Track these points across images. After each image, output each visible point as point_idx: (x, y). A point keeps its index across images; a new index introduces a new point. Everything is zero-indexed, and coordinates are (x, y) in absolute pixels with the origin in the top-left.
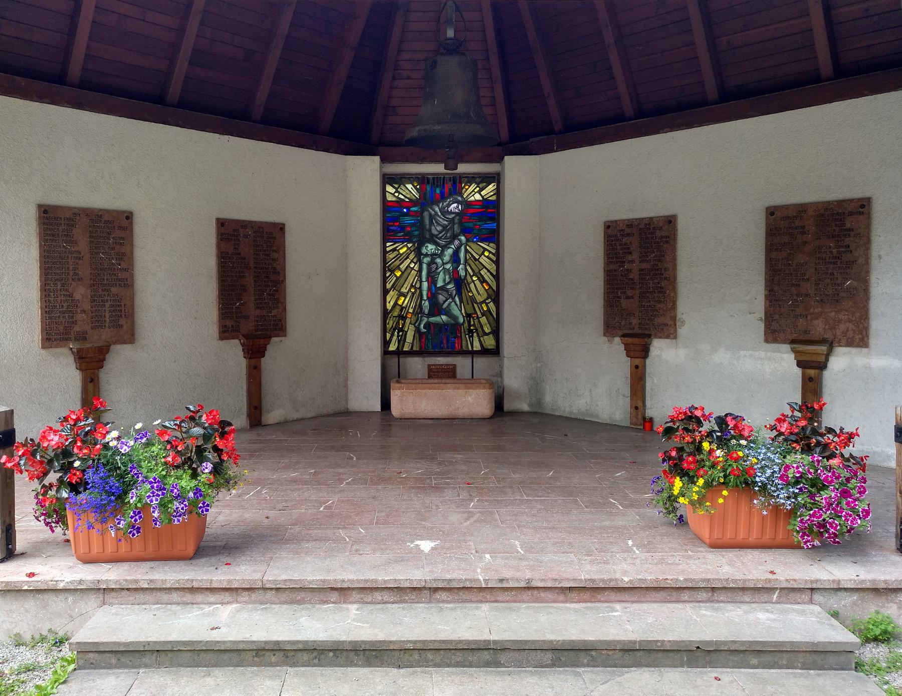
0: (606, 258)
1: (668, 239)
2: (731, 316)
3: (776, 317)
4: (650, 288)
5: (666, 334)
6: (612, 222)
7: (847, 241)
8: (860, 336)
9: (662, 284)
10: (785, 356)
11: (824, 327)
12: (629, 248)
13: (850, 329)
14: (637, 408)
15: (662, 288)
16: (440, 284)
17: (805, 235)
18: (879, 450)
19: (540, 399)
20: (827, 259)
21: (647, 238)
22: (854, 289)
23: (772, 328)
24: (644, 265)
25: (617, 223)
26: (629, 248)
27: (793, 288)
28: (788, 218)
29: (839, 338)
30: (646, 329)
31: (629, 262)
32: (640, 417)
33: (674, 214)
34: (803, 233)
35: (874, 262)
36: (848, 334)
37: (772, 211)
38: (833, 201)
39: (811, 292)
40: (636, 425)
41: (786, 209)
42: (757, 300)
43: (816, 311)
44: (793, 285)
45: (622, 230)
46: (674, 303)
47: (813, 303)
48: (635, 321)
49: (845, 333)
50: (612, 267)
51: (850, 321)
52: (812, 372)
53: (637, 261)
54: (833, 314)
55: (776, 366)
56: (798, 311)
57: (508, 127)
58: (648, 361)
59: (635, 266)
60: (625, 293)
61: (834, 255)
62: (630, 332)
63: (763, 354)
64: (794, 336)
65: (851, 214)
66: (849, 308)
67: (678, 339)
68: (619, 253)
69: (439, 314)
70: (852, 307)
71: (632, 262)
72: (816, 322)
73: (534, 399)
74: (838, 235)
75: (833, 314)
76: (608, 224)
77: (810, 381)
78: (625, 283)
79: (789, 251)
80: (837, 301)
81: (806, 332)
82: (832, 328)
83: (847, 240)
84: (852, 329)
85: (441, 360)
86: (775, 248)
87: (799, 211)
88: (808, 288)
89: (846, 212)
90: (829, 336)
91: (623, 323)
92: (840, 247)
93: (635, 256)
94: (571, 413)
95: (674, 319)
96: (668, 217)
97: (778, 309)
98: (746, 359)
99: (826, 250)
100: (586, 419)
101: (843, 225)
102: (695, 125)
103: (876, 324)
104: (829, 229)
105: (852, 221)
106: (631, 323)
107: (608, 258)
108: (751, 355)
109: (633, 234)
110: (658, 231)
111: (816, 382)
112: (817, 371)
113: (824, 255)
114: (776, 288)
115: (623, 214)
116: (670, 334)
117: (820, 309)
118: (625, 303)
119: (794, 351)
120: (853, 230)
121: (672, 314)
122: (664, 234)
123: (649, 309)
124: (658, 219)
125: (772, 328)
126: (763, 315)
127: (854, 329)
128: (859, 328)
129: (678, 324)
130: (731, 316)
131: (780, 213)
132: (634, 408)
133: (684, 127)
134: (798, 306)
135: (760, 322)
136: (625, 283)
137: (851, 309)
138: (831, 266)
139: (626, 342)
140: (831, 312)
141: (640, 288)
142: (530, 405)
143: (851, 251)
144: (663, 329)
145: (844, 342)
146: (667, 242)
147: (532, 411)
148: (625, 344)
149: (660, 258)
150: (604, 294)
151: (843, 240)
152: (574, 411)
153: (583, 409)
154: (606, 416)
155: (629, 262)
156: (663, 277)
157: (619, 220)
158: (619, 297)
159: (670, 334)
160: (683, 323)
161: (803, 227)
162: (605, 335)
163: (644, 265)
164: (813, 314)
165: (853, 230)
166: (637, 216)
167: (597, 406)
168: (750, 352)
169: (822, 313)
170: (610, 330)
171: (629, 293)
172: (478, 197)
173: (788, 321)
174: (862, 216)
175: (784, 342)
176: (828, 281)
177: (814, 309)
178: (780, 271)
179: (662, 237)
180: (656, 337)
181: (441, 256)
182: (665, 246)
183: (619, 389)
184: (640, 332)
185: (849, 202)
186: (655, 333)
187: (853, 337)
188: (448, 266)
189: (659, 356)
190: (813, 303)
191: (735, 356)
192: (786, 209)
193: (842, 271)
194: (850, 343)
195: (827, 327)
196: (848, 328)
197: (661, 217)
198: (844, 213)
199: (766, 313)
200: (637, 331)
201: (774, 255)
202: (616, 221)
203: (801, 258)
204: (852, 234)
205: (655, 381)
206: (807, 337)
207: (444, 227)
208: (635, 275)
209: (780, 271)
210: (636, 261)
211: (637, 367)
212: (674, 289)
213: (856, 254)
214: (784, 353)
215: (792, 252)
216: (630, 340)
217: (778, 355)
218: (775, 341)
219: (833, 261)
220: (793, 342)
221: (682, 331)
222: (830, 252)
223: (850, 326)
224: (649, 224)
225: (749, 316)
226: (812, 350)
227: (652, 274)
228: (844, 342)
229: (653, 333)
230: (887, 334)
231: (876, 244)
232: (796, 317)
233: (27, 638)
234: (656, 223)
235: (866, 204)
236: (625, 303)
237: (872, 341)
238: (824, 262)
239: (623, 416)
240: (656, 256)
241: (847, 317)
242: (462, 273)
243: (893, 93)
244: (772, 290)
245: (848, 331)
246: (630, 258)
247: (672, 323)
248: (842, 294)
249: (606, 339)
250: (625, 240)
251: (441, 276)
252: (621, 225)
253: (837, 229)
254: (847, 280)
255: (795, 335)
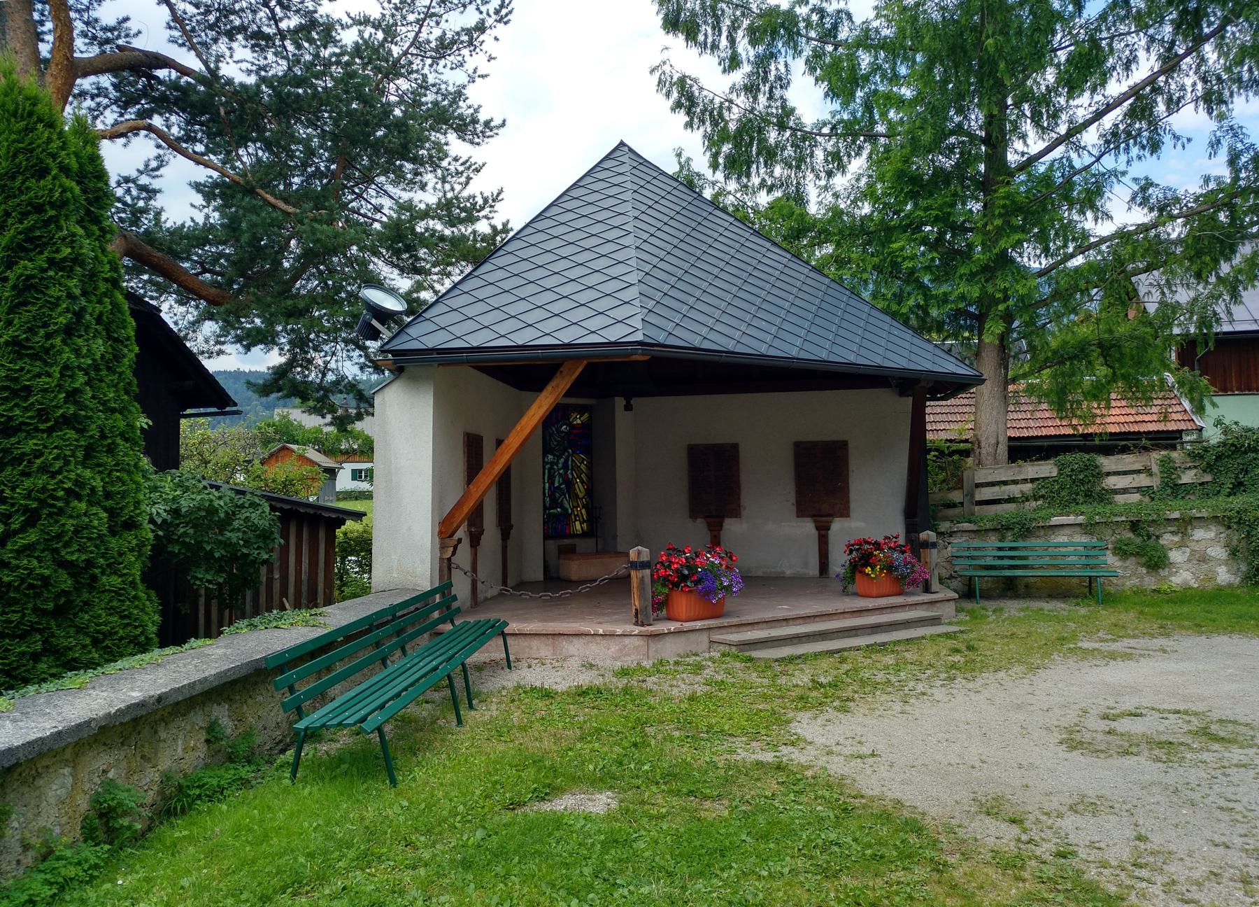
16: (556, 485)
35: (850, 473)
46: (739, 495)
52: (823, 532)
57: (534, 401)
69: (556, 508)
85: (566, 541)
90: (831, 512)
95: (739, 506)
103: (853, 505)
115: (700, 440)
119: (815, 521)
172: (579, 421)
175: (808, 516)
181: (557, 464)
188: (561, 471)
194: (842, 516)
207: (558, 442)
218: (803, 516)
220: (813, 516)
221: (744, 513)
233: (687, 119)
237: (851, 514)
242: (570, 476)
251: (557, 479)
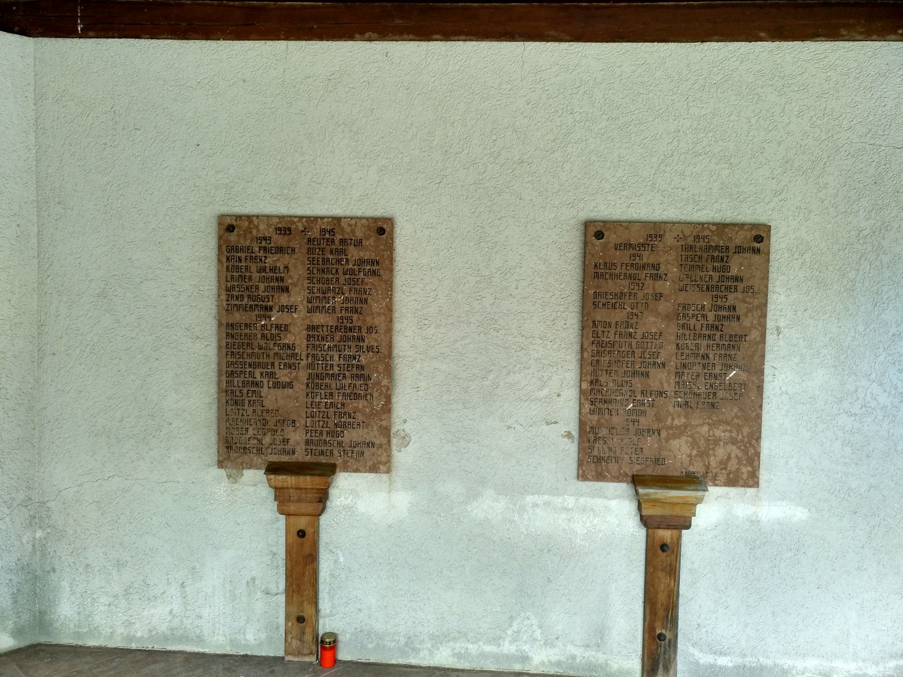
0: (224, 297)
1: (375, 267)
2: (509, 427)
3: (604, 432)
4: (332, 366)
5: (370, 463)
6: (239, 217)
7: (732, 298)
8: (750, 469)
9: (362, 359)
10: (614, 503)
11: (689, 452)
12: (282, 279)
13: (733, 455)
14: (301, 620)
15: (362, 368)
17: (661, 282)
18: (769, 662)
19: (42, 613)
20: (698, 327)
21: (326, 261)
22: (744, 385)
23: (595, 453)
24: (320, 319)
25: (251, 222)
26: (282, 279)
27: (637, 379)
28: (628, 246)
29: (714, 471)
30: (322, 453)
31: (282, 309)
32: (308, 637)
33: (386, 215)
34: (656, 277)
36: (729, 466)
37: (599, 229)
38: (709, 224)
39: (669, 388)
40: (300, 653)
41: (627, 228)
42: (561, 399)
43: (677, 422)
44: (634, 374)
45: (265, 239)
47: (671, 409)
48: (297, 437)
49: (724, 464)
50: (238, 317)
51: (734, 442)
52: (666, 535)
53: (302, 309)
54: (705, 428)
55: (595, 522)
56: (644, 422)
58: (324, 519)
59: (299, 320)
60: (272, 375)
61: (710, 322)
62: (285, 458)
63: (570, 501)
64: (636, 469)
65: (739, 250)
66: (733, 420)
67: (394, 473)
68: (257, 288)
70: (738, 418)
71: (290, 309)
72: (675, 443)
73: (26, 616)
74: (717, 287)
75: (705, 428)
76: (228, 221)
77: (663, 551)
78: (272, 353)
79: (629, 309)
80: (713, 405)
81: (657, 461)
82: (703, 454)
83: (731, 297)
84: (737, 457)
86: (604, 300)
87: (650, 236)
88: (661, 379)
89: (732, 246)
90: (697, 468)
91: (267, 440)
92: (720, 308)
93: (298, 297)
94: (131, 639)
96: (376, 220)
97: (607, 416)
98: (537, 510)
99: (696, 312)
100: (169, 648)
101: (726, 269)
102: (435, 37)
104: (702, 274)
105: (741, 264)
106: (286, 441)
107: (230, 297)
108: (547, 504)
109: (293, 250)
110: (351, 248)
111: (673, 551)
112: (675, 532)
113: (692, 322)
114: (603, 379)
116: (380, 463)
117: (683, 420)
118: (271, 397)
120: (742, 280)
121: (384, 423)
122: (366, 255)
123: (332, 410)
124: (353, 222)
125: (595, 453)
126: (574, 429)
127: (740, 455)
128: (747, 455)
129: (394, 441)
130: (509, 427)
131: (614, 236)
132: (295, 621)
133: (411, 36)
134: (644, 413)
135: (566, 440)
136: (272, 353)
137: (736, 421)
138: (704, 343)
139: (280, 485)
140: (702, 425)
141: (309, 366)
142: (17, 632)
143: (738, 318)
144: (362, 453)
145: (722, 478)
146: (374, 273)
147: (22, 644)
148: (276, 489)
149: (358, 306)
150: (220, 374)
151: (726, 297)
152: (139, 634)
153: (163, 628)
154: (221, 638)
155: (282, 309)
156: (365, 344)
157: (258, 217)
158: (256, 384)
159: (380, 463)
160: (406, 440)
161: (656, 267)
162: (220, 464)
163: (320, 319)
164: (671, 428)
165: (742, 280)
166: (299, 212)
167: (200, 617)
168: (546, 497)
169: (686, 426)
170: (233, 455)
171: (283, 375)
173: (625, 441)
174: (757, 257)
175: (618, 478)
176: (698, 369)
177: (673, 419)
178: (613, 345)
179: (361, 262)
180: (346, 469)
182: (370, 280)
183: (253, 579)
184: (308, 459)
185: (737, 228)
186: (345, 462)
187: (738, 470)
189: (349, 509)
190: (671, 409)
191: (515, 504)
192: (627, 228)
193: (723, 352)
194: (732, 481)
195: (694, 452)
196: (730, 454)
197: (360, 218)
198: (727, 248)
199: (582, 424)
200: (300, 456)
201: (600, 315)
202: (249, 218)
203: (651, 323)
204: (741, 286)
205: (342, 560)
206: (659, 471)
208: (297, 337)
209: (613, 345)
210: (300, 307)
211: (301, 534)
212: (389, 371)
213: (746, 322)
214: (610, 499)
215: (635, 311)
216: (288, 480)
217: (599, 502)
218: (600, 477)
219: (707, 332)
221: (402, 457)
222: (703, 316)
223: (735, 451)
224: (332, 231)
225: (545, 427)
226: (680, 497)
227: (338, 338)
228: (722, 478)
229: (339, 461)
230: (787, 463)
231: (773, 308)
232: (639, 432)
234: (348, 229)
235: (764, 235)
236: (271, 397)
238: (692, 333)
239: (263, 636)
240: (347, 300)
241: (728, 434)
243: (808, 43)
244: (597, 381)
245: (729, 458)
246: (284, 299)
247: (383, 440)
248: (721, 394)
249: (222, 472)
250: (270, 260)
252: (262, 227)
253: (716, 275)
254: (730, 367)
255: (639, 467)
